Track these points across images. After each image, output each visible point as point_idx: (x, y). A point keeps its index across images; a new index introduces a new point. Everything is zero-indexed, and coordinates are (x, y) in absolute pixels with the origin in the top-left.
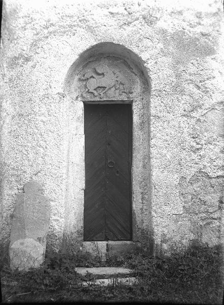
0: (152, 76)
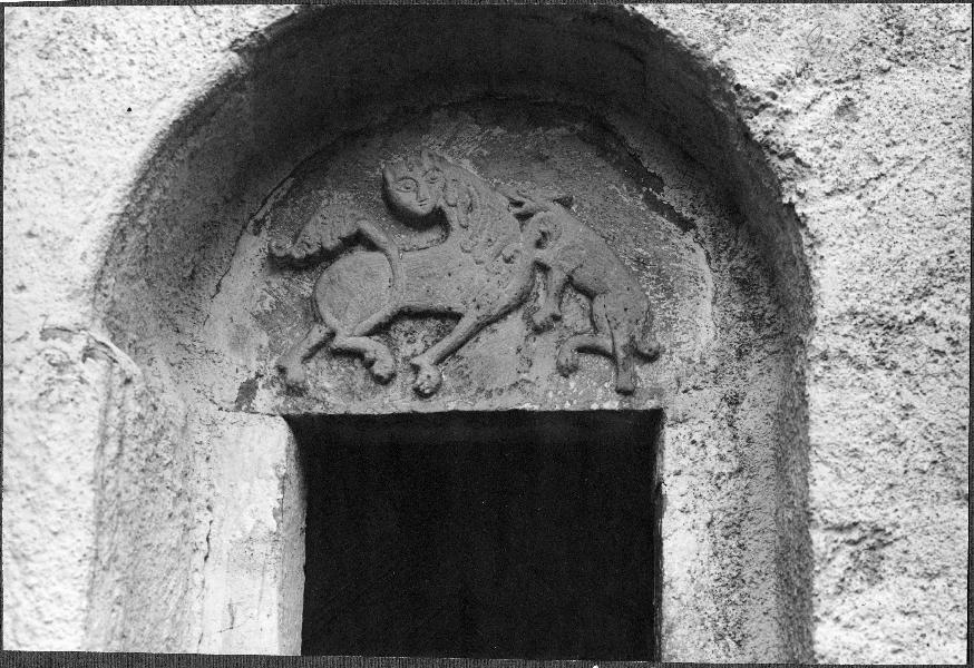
0: (821, 210)
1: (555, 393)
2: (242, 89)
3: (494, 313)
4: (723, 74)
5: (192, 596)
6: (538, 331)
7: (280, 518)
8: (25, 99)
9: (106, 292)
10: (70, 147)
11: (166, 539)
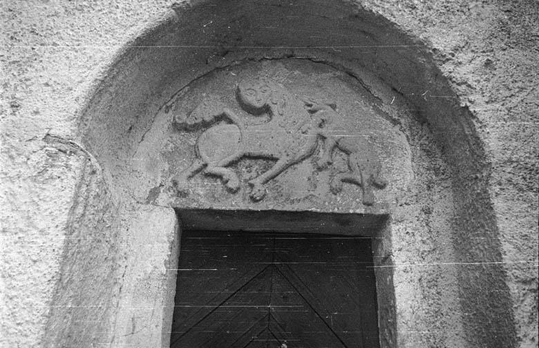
1: (329, 203)
2: (172, 31)
3: (296, 159)
4: (425, 44)
5: (111, 312)
6: (320, 169)
7: (168, 266)
8: (55, 18)
9: (86, 123)
10: (77, 43)
11: (102, 274)
